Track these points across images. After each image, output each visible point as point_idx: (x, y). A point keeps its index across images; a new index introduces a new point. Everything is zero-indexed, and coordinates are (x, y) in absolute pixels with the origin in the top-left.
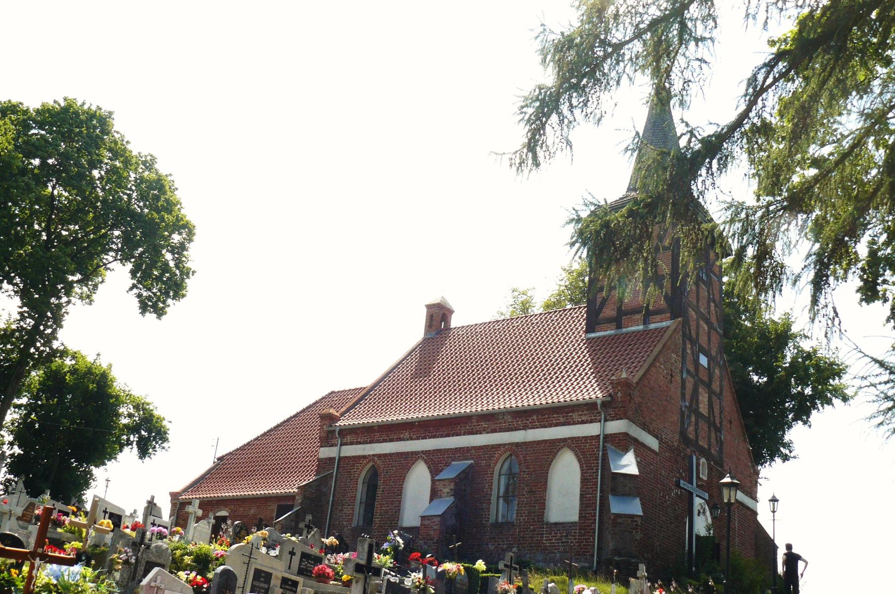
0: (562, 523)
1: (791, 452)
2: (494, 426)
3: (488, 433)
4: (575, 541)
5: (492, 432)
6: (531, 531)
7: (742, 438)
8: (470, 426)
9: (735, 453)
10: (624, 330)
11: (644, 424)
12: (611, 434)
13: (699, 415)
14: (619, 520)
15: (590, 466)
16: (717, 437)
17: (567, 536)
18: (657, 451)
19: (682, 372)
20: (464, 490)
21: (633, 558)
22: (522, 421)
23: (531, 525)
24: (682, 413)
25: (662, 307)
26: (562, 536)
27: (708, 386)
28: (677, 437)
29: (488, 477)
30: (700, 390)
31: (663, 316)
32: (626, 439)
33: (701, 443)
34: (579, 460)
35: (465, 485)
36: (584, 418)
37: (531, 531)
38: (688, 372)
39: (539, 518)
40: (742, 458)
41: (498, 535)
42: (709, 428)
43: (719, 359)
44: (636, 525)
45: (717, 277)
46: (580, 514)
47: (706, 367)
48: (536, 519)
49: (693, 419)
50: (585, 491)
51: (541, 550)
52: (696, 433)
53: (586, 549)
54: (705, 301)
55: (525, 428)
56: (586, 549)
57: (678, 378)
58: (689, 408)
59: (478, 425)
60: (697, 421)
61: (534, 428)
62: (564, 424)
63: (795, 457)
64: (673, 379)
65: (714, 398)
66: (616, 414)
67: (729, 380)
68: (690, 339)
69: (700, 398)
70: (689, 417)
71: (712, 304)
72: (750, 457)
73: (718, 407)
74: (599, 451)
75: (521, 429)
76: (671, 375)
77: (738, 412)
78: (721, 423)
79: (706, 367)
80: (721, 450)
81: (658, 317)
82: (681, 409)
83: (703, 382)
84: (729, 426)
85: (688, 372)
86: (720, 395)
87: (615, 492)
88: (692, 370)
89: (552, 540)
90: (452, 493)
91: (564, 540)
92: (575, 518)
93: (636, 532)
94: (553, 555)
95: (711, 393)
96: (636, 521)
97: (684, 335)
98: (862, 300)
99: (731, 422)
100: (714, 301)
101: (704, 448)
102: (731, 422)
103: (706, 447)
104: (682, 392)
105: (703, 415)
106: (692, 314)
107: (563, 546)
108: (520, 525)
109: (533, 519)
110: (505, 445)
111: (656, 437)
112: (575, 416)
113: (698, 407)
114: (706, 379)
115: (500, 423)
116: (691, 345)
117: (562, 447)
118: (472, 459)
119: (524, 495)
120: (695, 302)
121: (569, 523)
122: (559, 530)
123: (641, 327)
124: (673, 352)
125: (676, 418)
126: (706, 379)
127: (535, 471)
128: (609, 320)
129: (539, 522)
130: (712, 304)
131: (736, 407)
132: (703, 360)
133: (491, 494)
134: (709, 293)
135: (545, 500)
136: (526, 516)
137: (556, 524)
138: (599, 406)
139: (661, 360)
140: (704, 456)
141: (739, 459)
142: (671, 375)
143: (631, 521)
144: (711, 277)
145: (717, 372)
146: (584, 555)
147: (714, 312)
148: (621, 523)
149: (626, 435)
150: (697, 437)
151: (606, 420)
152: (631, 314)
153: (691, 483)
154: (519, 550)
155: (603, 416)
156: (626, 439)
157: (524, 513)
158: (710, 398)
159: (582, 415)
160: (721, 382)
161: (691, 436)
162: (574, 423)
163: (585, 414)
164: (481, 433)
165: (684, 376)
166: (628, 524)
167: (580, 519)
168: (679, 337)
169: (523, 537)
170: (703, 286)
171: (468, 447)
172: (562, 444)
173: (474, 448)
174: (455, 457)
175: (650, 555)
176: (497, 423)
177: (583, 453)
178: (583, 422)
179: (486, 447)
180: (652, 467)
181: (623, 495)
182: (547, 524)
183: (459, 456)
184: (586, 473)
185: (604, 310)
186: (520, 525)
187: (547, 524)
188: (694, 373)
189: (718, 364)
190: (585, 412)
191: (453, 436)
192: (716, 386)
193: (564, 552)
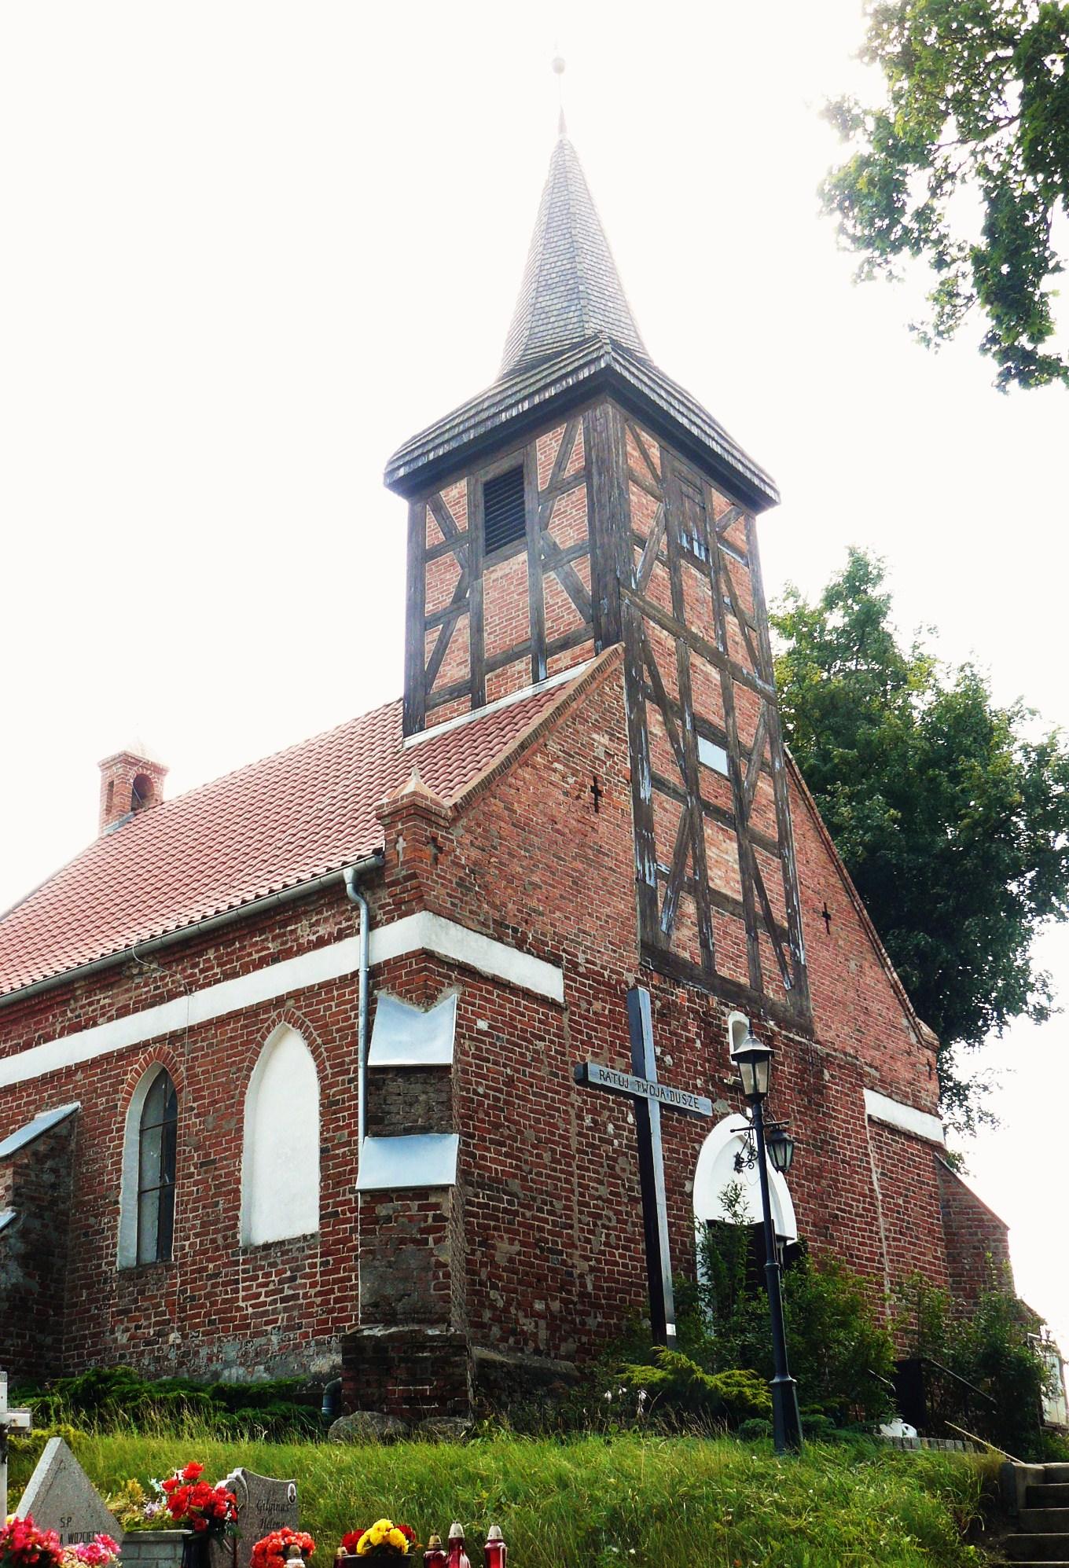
0: (281, 1243)
1: (1050, 998)
2: (122, 1000)
3: (110, 1019)
4: (313, 1291)
5: (119, 1016)
6: (209, 1277)
7: (871, 957)
8: (72, 1011)
9: (852, 994)
10: (490, 708)
11: (500, 924)
12: (387, 962)
13: (708, 898)
14: (382, 1210)
15: (342, 1064)
16: (781, 956)
17: (293, 1279)
18: (560, 999)
19: (634, 782)
20: (54, 1186)
21: (432, 1323)
22: (184, 970)
23: (209, 1260)
24: (648, 896)
25: (573, 627)
26: (281, 1282)
27: (737, 820)
28: (635, 958)
29: (112, 1140)
30: (708, 831)
31: (577, 649)
32: (425, 969)
33: (724, 972)
34: (315, 1052)
35: (54, 1171)
36: (323, 930)
37: (209, 1277)
38: (658, 783)
39: (225, 1238)
40: (875, 1007)
41: (136, 1301)
42: (751, 930)
43: (768, 755)
44: (436, 1218)
45: (741, 555)
46: (322, 1208)
47: (726, 773)
48: (220, 1242)
49: (690, 907)
50: (332, 1139)
51: (236, 1328)
52: (705, 944)
53: (343, 1310)
54: (706, 611)
55: (191, 987)
56: (343, 1310)
57: (625, 801)
58: (674, 879)
59: (90, 1004)
60: (704, 919)
61: (209, 985)
62: (275, 959)
63: (1059, 1010)
64: (603, 801)
65: (760, 855)
66: (398, 904)
67: (810, 808)
68: (659, 698)
69: (711, 852)
70: (674, 903)
71: (731, 620)
72: (902, 1003)
73: (779, 876)
74: (356, 1017)
75: (181, 994)
76: (596, 791)
77: (848, 891)
78: (792, 918)
79: (726, 773)
80: (799, 987)
81: (565, 657)
82: (640, 880)
83: (717, 813)
84: (821, 924)
85: (658, 783)
86: (780, 847)
87: (378, 1126)
88: (673, 777)
89: (259, 1295)
90: (9, 1197)
91: (288, 1292)
92: (311, 1224)
93: (437, 1241)
94: (263, 1340)
95: (747, 841)
96: (437, 1206)
97: (634, 685)
98: (1006, 376)
99: (827, 916)
100: (736, 612)
101: (739, 985)
102: (827, 916)
103: (744, 980)
104: (638, 835)
105: (726, 897)
106: (661, 638)
107: (285, 1310)
108: (183, 1265)
109: (213, 1241)
110: (145, 1044)
111: (555, 961)
112: (303, 930)
113: (705, 877)
114: (726, 803)
115: (138, 987)
116: (665, 714)
117: (274, 1023)
118: (78, 1096)
119: (191, 1175)
120: (668, 608)
121: (297, 1240)
122: (273, 1265)
123: (528, 692)
124: (597, 728)
125: (624, 904)
126: (726, 803)
127: (216, 1102)
128: (455, 692)
129: (226, 1247)
130: (731, 620)
131: (843, 879)
132: (713, 756)
133: (118, 1186)
134: (715, 587)
135: (238, 1181)
136: (197, 1235)
137: (267, 1247)
138: (349, 887)
139: (553, 747)
140: (740, 1007)
141: (867, 1011)
142: (596, 791)
143: (421, 1208)
144: (719, 552)
145: (765, 787)
146: (338, 1330)
147: (739, 638)
148: (388, 1219)
149: (426, 955)
150: (709, 955)
151: (372, 925)
152: (504, 664)
153: (638, 1070)
154: (184, 1337)
155: (363, 911)
156: (425, 969)
157: (194, 1227)
158: (744, 856)
159: (318, 922)
160: (780, 812)
161: (686, 955)
162: (302, 950)
163: (326, 920)
164: (95, 1024)
165: (646, 792)
166: (411, 1218)
167: (322, 1226)
168: (617, 693)
169: (193, 1298)
170: (694, 571)
171: (68, 1068)
172: (274, 1014)
173: (82, 1066)
174: (42, 1099)
175: (556, 1306)
176: (127, 991)
177: (324, 1030)
178: (321, 943)
179: (106, 1058)
180: (540, 1045)
181: (408, 1131)
182: (245, 1252)
183: (50, 1096)
184: (331, 1086)
185: (441, 669)
186: (183, 1265)
187: (245, 1252)
188: (682, 789)
189: (765, 766)
190: (325, 914)
191: (38, 1044)
192: (763, 823)
193: (288, 1328)
